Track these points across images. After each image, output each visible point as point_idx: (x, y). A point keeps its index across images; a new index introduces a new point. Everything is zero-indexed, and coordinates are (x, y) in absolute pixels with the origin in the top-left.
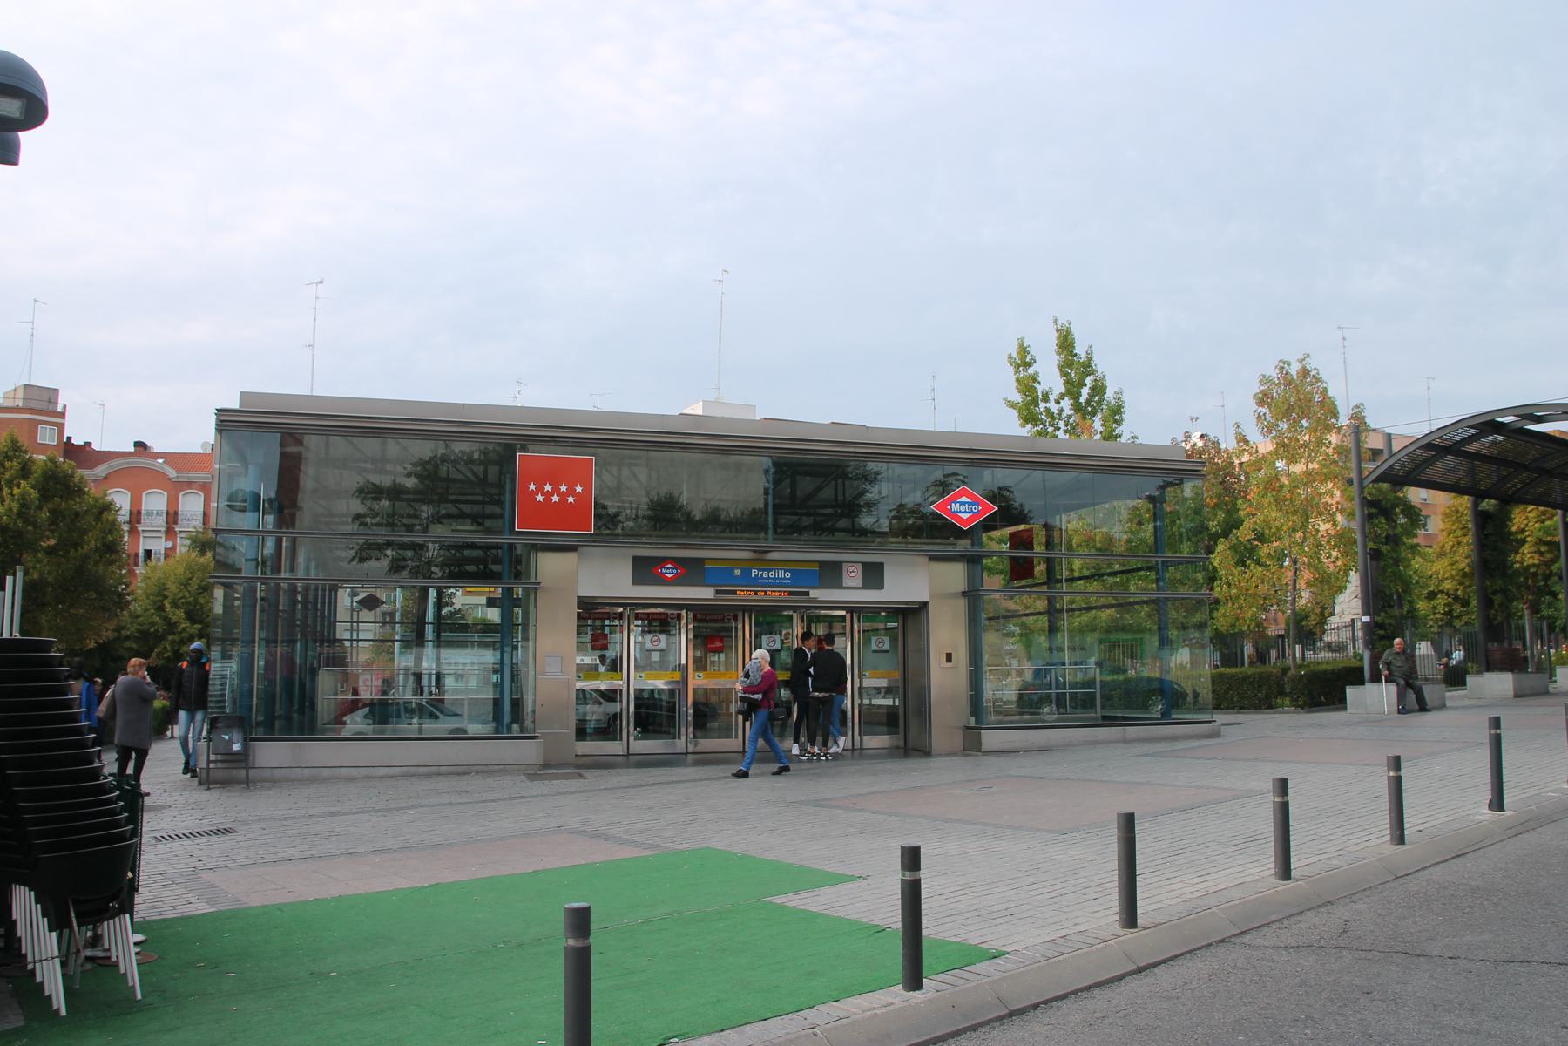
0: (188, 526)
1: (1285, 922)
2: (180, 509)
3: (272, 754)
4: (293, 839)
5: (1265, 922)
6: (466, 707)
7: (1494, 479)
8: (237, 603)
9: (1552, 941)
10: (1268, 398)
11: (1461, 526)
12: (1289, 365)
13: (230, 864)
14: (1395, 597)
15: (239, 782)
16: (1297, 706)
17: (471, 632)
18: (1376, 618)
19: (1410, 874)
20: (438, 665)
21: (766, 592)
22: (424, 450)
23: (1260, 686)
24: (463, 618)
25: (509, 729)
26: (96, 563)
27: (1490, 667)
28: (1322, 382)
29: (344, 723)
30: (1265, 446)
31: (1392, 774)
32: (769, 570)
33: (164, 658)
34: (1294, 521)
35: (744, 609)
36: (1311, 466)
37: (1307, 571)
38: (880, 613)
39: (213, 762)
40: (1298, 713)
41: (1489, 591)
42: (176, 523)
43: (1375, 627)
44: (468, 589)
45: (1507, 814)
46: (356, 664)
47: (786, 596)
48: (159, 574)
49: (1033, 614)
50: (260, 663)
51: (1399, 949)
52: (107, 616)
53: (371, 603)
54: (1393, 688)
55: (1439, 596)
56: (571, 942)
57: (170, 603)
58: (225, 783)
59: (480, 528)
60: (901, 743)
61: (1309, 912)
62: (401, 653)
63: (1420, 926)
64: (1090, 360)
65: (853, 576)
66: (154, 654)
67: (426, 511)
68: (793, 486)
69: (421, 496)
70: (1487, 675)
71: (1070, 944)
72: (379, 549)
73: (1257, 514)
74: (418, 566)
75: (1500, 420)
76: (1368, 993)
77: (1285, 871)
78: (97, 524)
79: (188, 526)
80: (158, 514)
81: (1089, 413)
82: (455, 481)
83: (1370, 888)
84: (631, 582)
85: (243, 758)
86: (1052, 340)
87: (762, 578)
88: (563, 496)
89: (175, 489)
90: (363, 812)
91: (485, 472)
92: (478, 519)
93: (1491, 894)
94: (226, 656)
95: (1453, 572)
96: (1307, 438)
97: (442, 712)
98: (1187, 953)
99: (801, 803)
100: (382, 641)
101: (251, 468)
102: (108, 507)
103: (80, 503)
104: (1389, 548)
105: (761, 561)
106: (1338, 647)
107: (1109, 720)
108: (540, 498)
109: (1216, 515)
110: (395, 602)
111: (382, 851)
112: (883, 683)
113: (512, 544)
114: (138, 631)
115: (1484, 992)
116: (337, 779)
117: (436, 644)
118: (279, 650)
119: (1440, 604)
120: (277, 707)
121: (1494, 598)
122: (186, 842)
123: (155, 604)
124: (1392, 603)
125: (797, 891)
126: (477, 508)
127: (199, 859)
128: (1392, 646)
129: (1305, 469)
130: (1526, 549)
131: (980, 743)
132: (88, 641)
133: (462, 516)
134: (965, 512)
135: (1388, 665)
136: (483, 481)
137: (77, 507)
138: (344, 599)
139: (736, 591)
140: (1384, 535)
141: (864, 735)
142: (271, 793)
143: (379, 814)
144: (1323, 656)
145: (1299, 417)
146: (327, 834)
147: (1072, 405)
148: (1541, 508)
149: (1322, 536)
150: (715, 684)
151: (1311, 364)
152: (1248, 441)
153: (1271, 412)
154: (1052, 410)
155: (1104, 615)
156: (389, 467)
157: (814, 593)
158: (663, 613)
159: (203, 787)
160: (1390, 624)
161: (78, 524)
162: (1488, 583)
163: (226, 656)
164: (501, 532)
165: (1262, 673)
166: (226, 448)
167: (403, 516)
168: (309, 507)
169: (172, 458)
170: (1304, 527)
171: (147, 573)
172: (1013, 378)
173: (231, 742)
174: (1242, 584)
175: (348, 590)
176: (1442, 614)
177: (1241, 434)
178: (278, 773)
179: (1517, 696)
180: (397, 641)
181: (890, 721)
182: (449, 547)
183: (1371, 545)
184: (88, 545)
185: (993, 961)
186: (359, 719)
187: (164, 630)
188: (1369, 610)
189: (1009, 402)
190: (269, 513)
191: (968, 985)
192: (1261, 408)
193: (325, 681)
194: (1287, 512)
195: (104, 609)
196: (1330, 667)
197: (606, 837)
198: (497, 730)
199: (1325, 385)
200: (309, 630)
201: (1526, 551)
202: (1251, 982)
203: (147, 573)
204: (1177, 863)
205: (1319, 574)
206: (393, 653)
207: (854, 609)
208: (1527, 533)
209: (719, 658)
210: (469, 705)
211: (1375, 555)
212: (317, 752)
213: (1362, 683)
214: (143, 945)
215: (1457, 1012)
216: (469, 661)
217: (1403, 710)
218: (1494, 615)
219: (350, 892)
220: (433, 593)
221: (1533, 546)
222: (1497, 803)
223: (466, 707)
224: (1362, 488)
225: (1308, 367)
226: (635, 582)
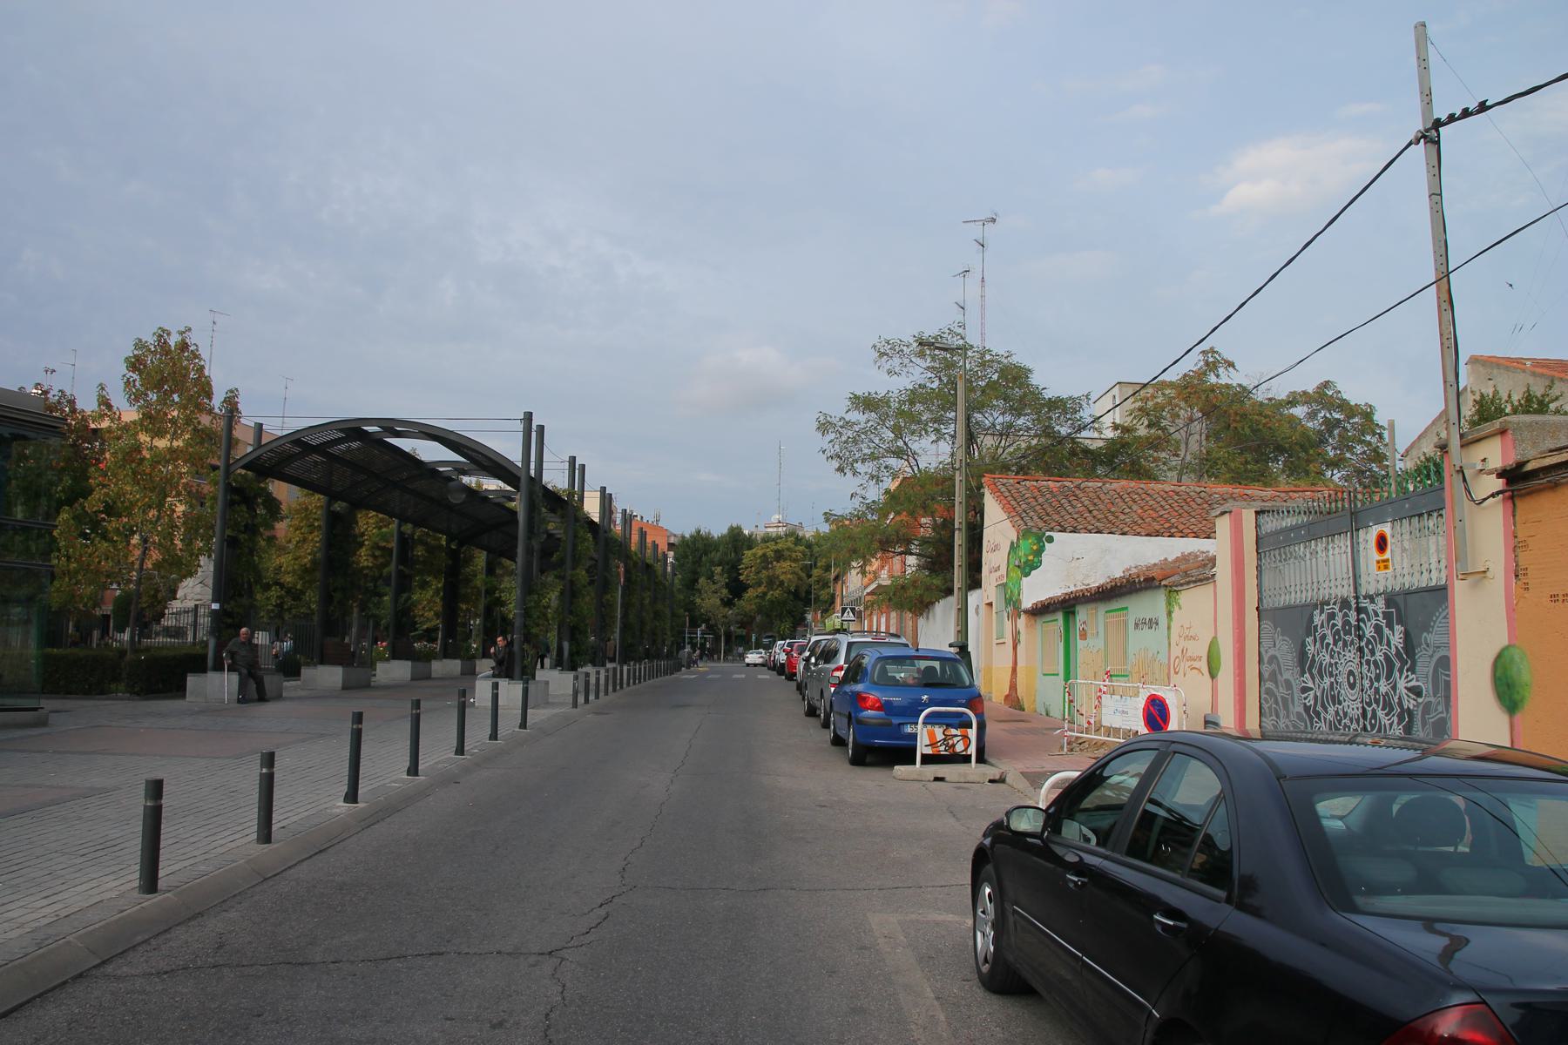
1: (153, 942)
9: (420, 931)
12: (169, 334)
19: (278, 874)
28: (200, 359)
30: (130, 414)
34: (150, 498)
36: (175, 444)
37: (157, 552)
40: (133, 700)
45: (361, 805)
51: (281, 959)
54: (235, 677)
55: (273, 589)
61: (178, 928)
63: (297, 930)
75: (365, 428)
76: (259, 1016)
83: (240, 893)
95: (296, 567)
96: (175, 413)
98: (34, 998)
104: (246, 537)
106: (178, 632)
109: (61, 480)
115: (372, 995)
128: (238, 635)
130: (363, 551)
135: (232, 655)
140: (243, 524)
144: (161, 640)
148: (381, 516)
149: (178, 517)
151: (193, 339)
153: (141, 378)
170: (160, 506)
183: (228, 532)
192: (131, 374)
194: (145, 488)
199: (202, 363)
202: (122, 1023)
204: (13, 882)
205: (169, 555)
211: (232, 542)
213: (204, 671)
215: (352, 1022)
218: (332, 611)
222: (352, 796)
224: (228, 473)
225: (188, 341)
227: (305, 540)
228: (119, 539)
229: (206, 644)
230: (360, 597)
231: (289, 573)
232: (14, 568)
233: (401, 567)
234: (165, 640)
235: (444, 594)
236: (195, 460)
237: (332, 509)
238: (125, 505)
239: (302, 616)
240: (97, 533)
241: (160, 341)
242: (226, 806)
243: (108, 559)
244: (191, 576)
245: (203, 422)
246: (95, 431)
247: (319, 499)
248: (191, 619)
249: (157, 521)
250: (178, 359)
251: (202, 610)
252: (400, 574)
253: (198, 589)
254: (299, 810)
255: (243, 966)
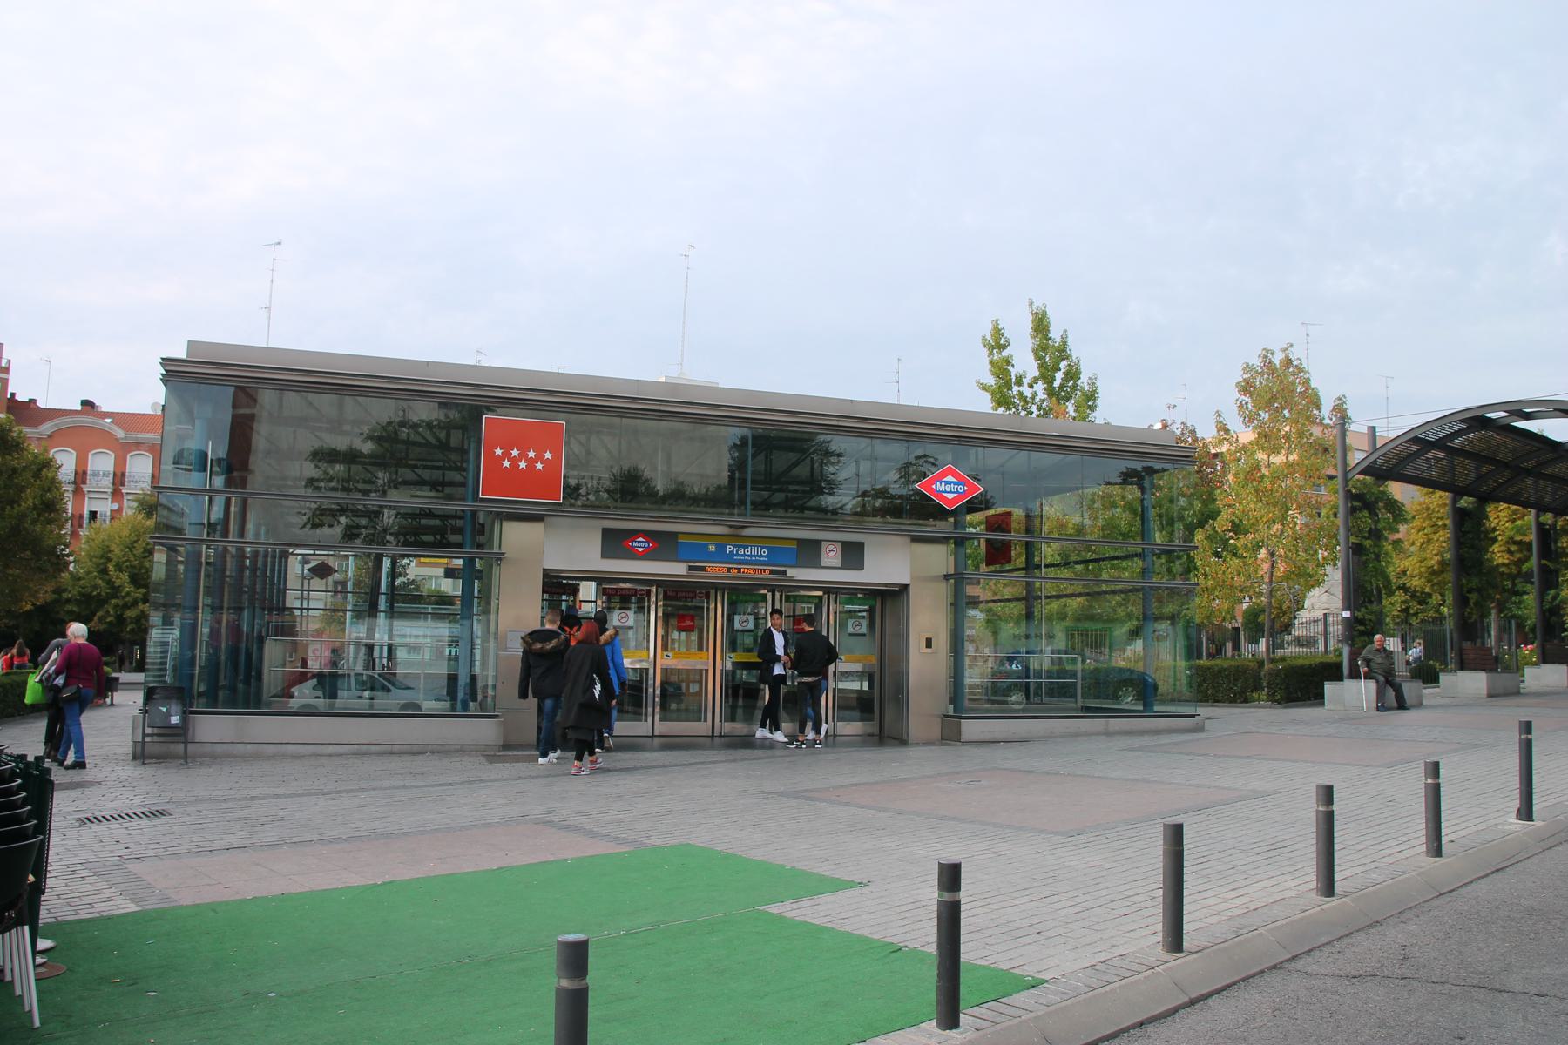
0: (136, 489)
2: (127, 471)
3: (212, 728)
4: (232, 824)
5: (1315, 945)
6: (422, 681)
7: (1472, 477)
8: (181, 567)
10: (1251, 387)
11: (1431, 523)
12: (1273, 354)
13: (161, 853)
14: (1375, 592)
15: (175, 757)
16: (1272, 701)
17: (424, 604)
18: (1357, 614)
20: (390, 638)
21: (739, 570)
22: (383, 411)
23: (1236, 680)
24: (417, 588)
25: (465, 707)
26: (34, 522)
27: (1463, 666)
28: (1305, 372)
29: (292, 696)
30: (1246, 435)
31: (1430, 781)
32: (745, 547)
33: (105, 623)
35: (716, 587)
36: (1291, 458)
37: (1283, 564)
38: (856, 594)
39: (148, 735)
41: (1465, 589)
42: (123, 484)
43: (1355, 623)
44: (423, 560)
45: (1537, 823)
46: (306, 633)
47: (766, 575)
48: (102, 536)
49: (1000, 601)
50: (204, 630)
51: (1475, 983)
52: (44, 577)
53: (322, 571)
54: (1372, 685)
55: (1397, 593)
56: (565, 983)
57: (115, 566)
58: (161, 758)
59: (440, 495)
60: (876, 730)
62: (352, 623)
64: (1065, 344)
65: (831, 555)
66: (96, 618)
67: (382, 477)
68: (768, 461)
69: (377, 461)
70: (1461, 674)
71: (1113, 970)
72: (333, 516)
73: (1234, 501)
74: (373, 535)
75: (1487, 415)
77: (1328, 887)
78: (35, 481)
79: (136, 489)
80: (104, 474)
81: (1063, 398)
82: (415, 443)
84: (600, 556)
85: (182, 732)
86: (1027, 324)
87: (737, 555)
88: (531, 462)
89: (123, 450)
90: (310, 794)
91: (448, 435)
92: (435, 485)
93: (1551, 917)
94: (167, 622)
95: (1422, 570)
96: (1287, 429)
97: (394, 685)
98: (1238, 981)
99: (781, 794)
100: (334, 610)
101: (197, 422)
102: (48, 464)
103: (18, 459)
105: (737, 538)
106: (1309, 642)
107: (1089, 712)
108: (506, 464)
110: (347, 571)
111: (330, 841)
112: (857, 667)
113: (476, 511)
114: (80, 594)
116: (284, 756)
117: (389, 615)
118: (225, 617)
119: (1397, 601)
120: (222, 676)
121: (1470, 596)
122: (114, 825)
123: (98, 566)
124: (1373, 599)
125: (795, 898)
126: (437, 475)
127: (127, 845)
128: (1372, 642)
129: (1285, 461)
130: (1496, 547)
131: (959, 733)
132: (24, 603)
133: (420, 483)
134: (951, 492)
135: (1368, 662)
136: (444, 446)
137: (15, 463)
138: (295, 567)
139: (705, 567)
140: (1367, 530)
141: (838, 721)
142: (211, 770)
143: (328, 796)
145: (1282, 406)
146: (270, 819)
147: (1045, 389)
148: (1514, 507)
150: (683, 665)
151: (1295, 354)
152: (1229, 430)
153: (1253, 400)
154: (1025, 394)
155: (1074, 603)
156: (347, 428)
157: (791, 572)
158: (633, 589)
159: (137, 762)
160: (1370, 620)
161: (16, 480)
162: (1464, 581)
163: (167, 622)
164: (464, 499)
165: (1238, 666)
166: (175, 407)
167: (358, 482)
168: (261, 467)
169: (120, 418)
170: (1284, 518)
171: (91, 535)
172: (987, 360)
173: (168, 714)
174: (1219, 576)
175: (299, 557)
176: (1399, 611)
177: (1221, 422)
178: (219, 749)
179: (1490, 695)
180: (349, 610)
181: (863, 706)
182: (405, 515)
183: (1353, 539)
184: (26, 503)
185: (1032, 991)
186: (307, 692)
187: (107, 593)
188: (1350, 606)
189: (982, 384)
190: (217, 474)
191: (1010, 1023)
192: (1243, 397)
193: (273, 651)
195: (42, 570)
196: (1307, 662)
197: (575, 829)
198: (453, 708)
199: (1306, 376)
200: (257, 596)
201: (1496, 551)
203: (91, 535)
206: (344, 623)
207: (832, 590)
208: (1498, 533)
209: (679, 636)
210: (425, 678)
211: (1357, 549)
212: (260, 727)
213: (1340, 679)
214: (52, 953)
216: (421, 633)
217: (1382, 707)
218: (1469, 613)
219: (295, 889)
220: (387, 563)
221: (1504, 545)
222: (1526, 812)
223: (422, 681)
224: (1346, 481)
225: (1291, 357)
226: (604, 556)
227: (1429, 541)
228: (1248, 555)
229: (1339, 653)
230: (1498, 596)
231: (1416, 576)
232: (1159, 588)
233: (1544, 562)
234: (1297, 650)
235: (602, 686)
236: (1311, 476)
237: (1458, 506)
238: (1251, 521)
239: (1431, 620)
240: (1227, 551)
241: (1265, 361)
242: (1385, 815)
243: (1240, 574)
244: (1319, 585)
245: (1315, 433)
246: (1216, 455)
247: (1441, 497)
248: (1320, 628)
249: (1281, 535)
250: (1285, 375)
251: (1331, 619)
252: (1544, 570)
253: (1324, 598)
254: (1466, 824)
255: (1433, 982)
